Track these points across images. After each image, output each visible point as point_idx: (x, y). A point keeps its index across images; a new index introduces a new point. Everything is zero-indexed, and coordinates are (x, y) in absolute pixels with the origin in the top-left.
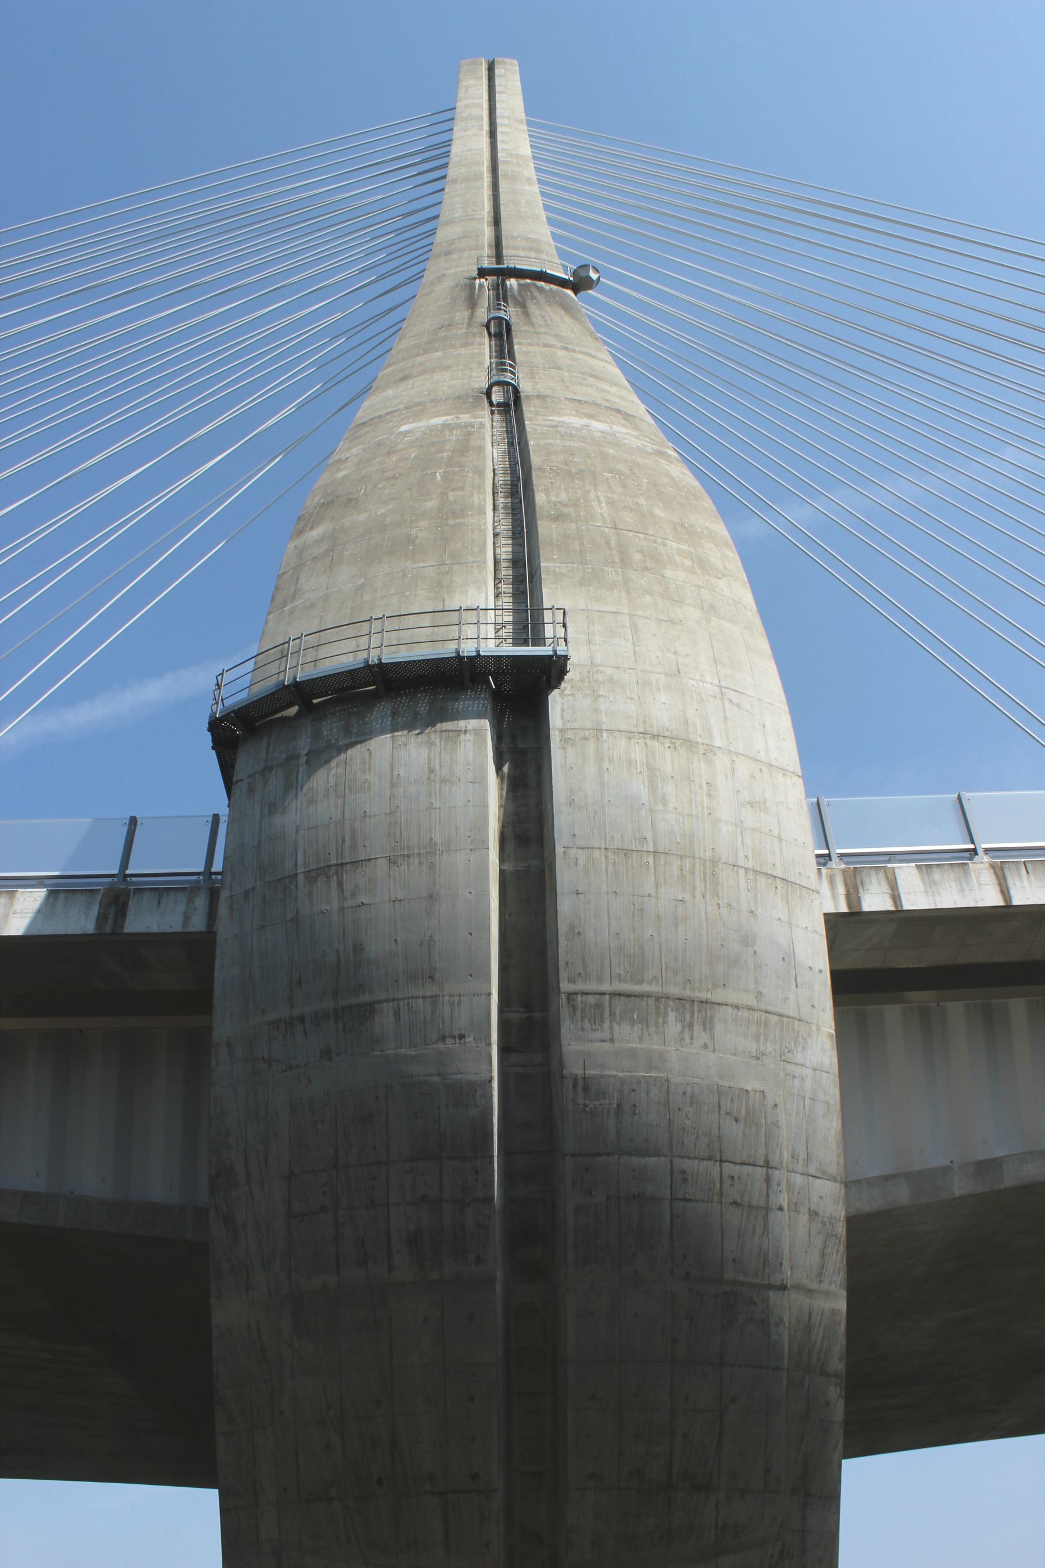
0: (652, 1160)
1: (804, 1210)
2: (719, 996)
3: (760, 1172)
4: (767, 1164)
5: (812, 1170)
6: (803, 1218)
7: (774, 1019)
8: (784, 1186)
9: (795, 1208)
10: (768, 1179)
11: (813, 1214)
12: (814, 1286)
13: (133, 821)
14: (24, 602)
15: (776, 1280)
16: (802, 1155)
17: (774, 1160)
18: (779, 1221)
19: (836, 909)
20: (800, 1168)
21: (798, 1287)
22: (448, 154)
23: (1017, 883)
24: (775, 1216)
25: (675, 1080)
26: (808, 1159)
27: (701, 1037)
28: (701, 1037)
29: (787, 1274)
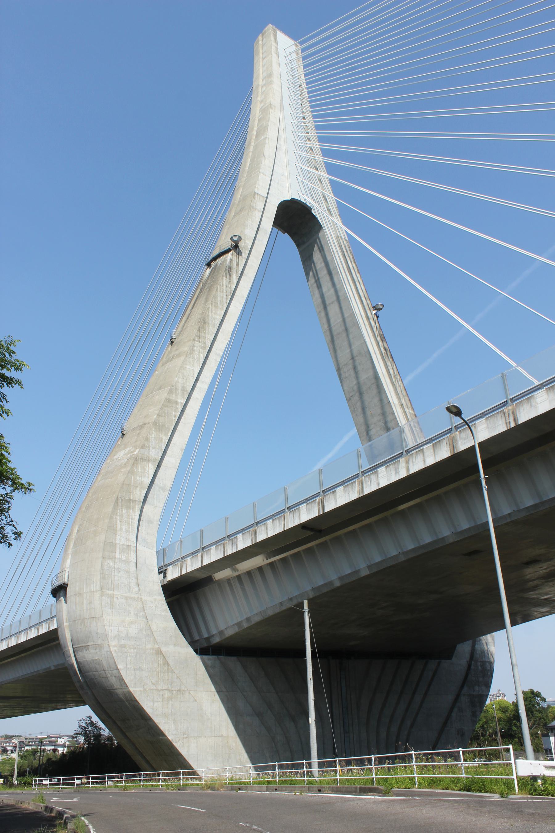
0: (90, 673)
1: (113, 676)
2: (89, 644)
3: (104, 672)
4: (104, 670)
5: (112, 669)
6: (114, 678)
7: (97, 645)
8: (108, 673)
9: (111, 676)
10: (105, 673)
11: (115, 676)
12: (121, 688)
13: (227, 519)
14: (424, 247)
15: (114, 688)
16: (109, 668)
17: (105, 670)
18: (110, 679)
19: (379, 486)
20: (109, 669)
21: (119, 689)
22: (306, 53)
23: (368, 483)
24: (109, 678)
25: (87, 660)
26: (110, 668)
27: (88, 652)
28: (88, 652)
29: (115, 687)
